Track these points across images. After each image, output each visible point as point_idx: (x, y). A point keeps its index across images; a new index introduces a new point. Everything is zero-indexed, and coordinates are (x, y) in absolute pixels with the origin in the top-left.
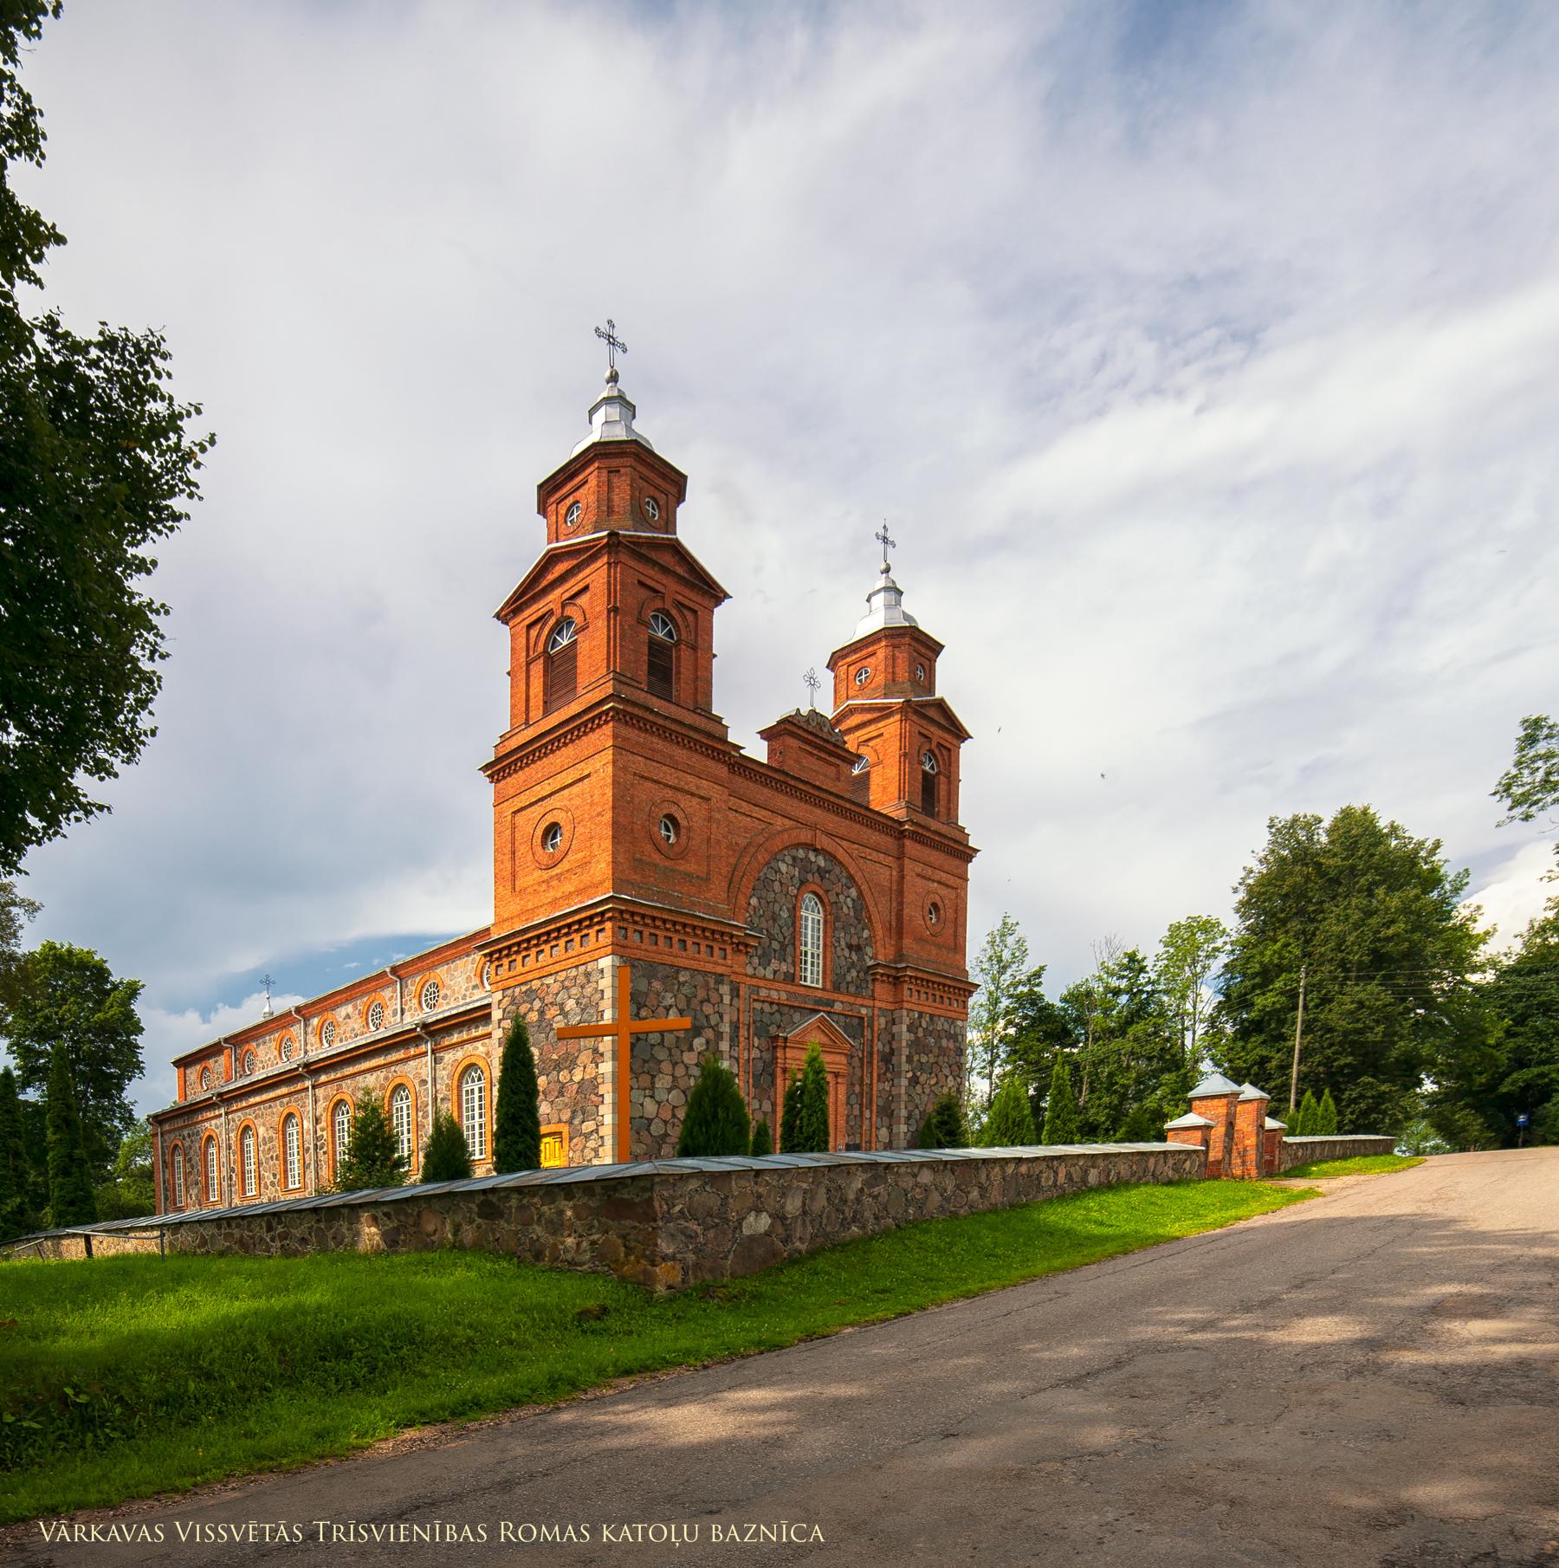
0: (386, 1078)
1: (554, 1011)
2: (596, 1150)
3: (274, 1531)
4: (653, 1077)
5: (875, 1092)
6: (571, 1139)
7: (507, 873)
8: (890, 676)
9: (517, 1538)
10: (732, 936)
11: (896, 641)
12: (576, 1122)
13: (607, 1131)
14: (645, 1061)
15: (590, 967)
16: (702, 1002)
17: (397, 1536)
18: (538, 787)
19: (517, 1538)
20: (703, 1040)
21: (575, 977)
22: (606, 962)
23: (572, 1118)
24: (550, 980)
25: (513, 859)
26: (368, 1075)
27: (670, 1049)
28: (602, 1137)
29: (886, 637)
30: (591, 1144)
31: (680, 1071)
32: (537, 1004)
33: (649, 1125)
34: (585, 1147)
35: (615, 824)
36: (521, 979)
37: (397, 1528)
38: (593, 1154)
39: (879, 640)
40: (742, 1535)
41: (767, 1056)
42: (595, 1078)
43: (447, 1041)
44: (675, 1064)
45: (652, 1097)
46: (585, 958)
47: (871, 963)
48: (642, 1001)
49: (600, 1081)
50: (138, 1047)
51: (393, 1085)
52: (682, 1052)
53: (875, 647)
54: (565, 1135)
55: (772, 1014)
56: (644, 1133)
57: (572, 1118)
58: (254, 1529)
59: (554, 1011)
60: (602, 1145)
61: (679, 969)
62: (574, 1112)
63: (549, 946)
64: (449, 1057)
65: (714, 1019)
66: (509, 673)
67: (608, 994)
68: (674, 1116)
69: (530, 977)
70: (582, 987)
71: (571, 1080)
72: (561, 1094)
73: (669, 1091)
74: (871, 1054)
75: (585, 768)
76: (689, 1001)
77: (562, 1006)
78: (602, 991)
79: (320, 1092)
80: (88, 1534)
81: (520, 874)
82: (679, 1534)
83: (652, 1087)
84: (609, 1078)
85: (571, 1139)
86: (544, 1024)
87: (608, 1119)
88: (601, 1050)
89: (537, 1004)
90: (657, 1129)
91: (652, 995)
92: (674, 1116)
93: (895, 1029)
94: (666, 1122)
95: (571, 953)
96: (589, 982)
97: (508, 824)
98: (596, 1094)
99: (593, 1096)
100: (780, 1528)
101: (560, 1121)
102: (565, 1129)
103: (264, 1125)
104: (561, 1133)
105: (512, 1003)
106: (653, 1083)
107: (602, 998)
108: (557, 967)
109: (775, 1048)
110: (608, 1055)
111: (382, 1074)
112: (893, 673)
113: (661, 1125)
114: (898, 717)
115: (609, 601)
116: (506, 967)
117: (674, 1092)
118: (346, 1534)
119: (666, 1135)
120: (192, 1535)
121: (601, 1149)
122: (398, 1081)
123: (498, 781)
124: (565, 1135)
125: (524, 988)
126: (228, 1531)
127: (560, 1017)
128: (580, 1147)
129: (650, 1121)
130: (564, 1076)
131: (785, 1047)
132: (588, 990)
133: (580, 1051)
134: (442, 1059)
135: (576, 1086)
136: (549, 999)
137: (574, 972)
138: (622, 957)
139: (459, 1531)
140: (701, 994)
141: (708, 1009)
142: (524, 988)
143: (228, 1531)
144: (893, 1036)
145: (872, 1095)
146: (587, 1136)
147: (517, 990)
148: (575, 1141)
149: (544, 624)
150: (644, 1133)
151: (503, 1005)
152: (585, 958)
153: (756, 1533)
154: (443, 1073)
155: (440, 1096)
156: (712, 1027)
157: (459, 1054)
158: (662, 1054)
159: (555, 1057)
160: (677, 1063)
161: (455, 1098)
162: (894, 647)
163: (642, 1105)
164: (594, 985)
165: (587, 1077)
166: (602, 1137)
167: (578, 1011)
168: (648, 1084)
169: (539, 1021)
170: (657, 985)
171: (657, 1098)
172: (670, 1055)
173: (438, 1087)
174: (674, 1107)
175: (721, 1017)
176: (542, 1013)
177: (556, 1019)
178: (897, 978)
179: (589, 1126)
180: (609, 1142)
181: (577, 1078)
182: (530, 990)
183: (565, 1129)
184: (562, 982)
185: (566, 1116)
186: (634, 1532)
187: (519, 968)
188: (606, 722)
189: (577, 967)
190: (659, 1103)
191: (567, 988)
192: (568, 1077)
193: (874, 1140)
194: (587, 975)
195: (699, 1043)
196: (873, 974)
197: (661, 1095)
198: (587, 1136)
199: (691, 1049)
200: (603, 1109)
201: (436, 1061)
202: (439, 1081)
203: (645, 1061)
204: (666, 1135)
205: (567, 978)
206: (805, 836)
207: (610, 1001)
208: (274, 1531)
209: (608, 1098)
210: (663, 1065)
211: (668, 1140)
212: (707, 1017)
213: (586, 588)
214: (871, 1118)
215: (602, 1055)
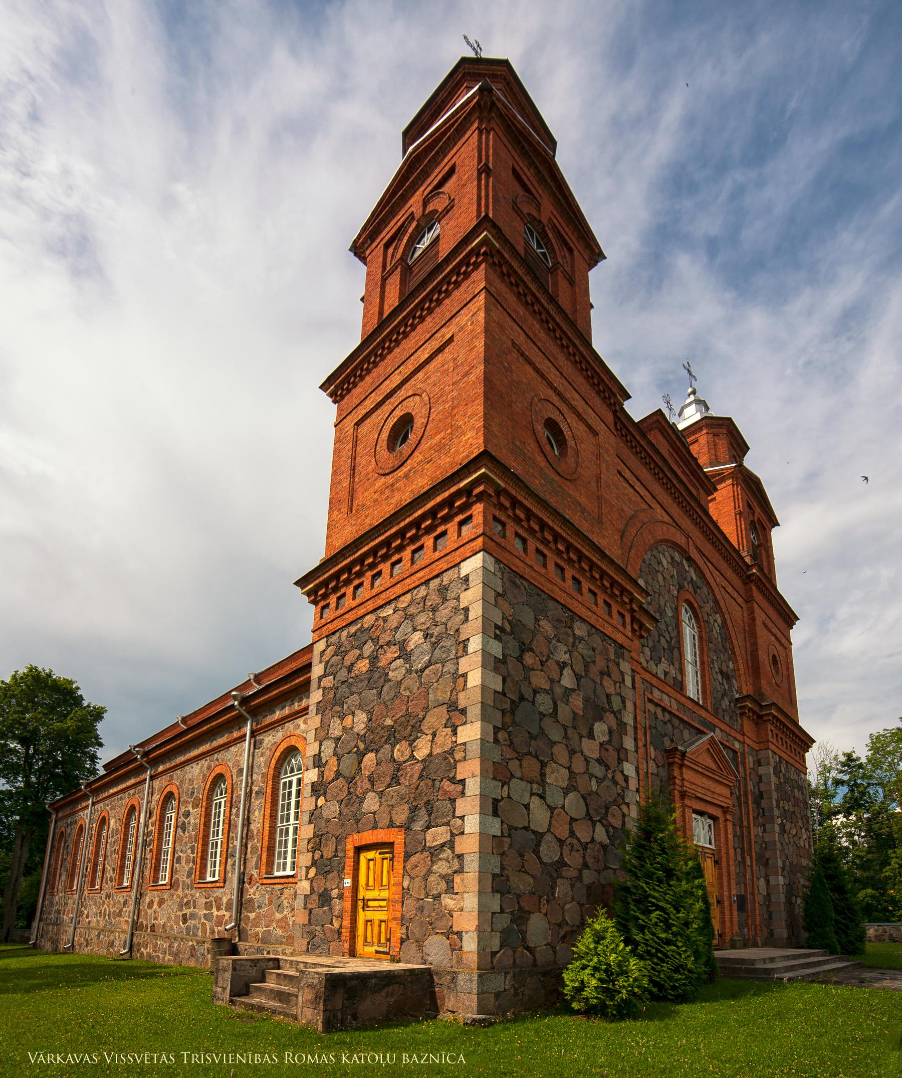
0: (209, 768)
1: (392, 652)
2: (449, 880)
3: (159, 1059)
4: (543, 765)
5: (752, 837)
6: (407, 856)
7: (344, 495)
8: (713, 457)
9: (294, 1061)
10: (632, 600)
11: (716, 431)
12: (417, 827)
13: (469, 845)
14: (532, 737)
15: (446, 578)
16: (602, 674)
17: (227, 1061)
18: (387, 382)
19: (294, 1061)
20: (605, 727)
21: (424, 599)
22: (473, 565)
23: (411, 820)
24: (388, 611)
25: (353, 476)
26: (194, 765)
27: (565, 728)
28: (460, 857)
29: (707, 426)
30: (441, 867)
31: (579, 766)
32: (369, 649)
33: (538, 844)
34: (429, 872)
35: (488, 379)
36: (350, 617)
37: (227, 1057)
38: (443, 886)
39: (700, 429)
40: (420, 1058)
41: (663, 773)
42: (451, 752)
43: (269, 719)
44: (572, 752)
45: (542, 797)
46: (442, 565)
47: (737, 696)
48: (527, 642)
49: (458, 756)
50: (97, 758)
51: (213, 775)
52: (581, 737)
53: (696, 436)
54: (399, 849)
55: (665, 723)
56: (530, 856)
57: (411, 820)
58: (148, 1056)
59: (392, 652)
60: (460, 871)
61: (574, 616)
62: (414, 810)
63: (388, 564)
64: (268, 739)
65: (616, 702)
66: (362, 299)
67: (476, 611)
68: (572, 834)
69: (361, 611)
70: (434, 610)
71: (412, 757)
72: (395, 780)
73: (566, 792)
74: (746, 794)
75: (447, 333)
76: (586, 666)
77: (403, 645)
78: (466, 610)
79: (157, 783)
80: (55, 1059)
81: (359, 489)
82: (385, 1058)
83: (542, 782)
84: (475, 750)
85: (407, 856)
86: (376, 675)
87: (472, 824)
88: (462, 704)
89: (369, 649)
90: (549, 852)
91: (540, 638)
92: (572, 834)
93: (762, 770)
94: (561, 842)
95: (419, 564)
96: (445, 600)
97: (350, 438)
98: (453, 780)
99: (446, 784)
100: (441, 1055)
101: (391, 825)
102: (398, 838)
103: (115, 817)
104: (391, 845)
105: (336, 654)
106: (543, 775)
107: (466, 620)
108: (398, 590)
109: (670, 765)
110: (475, 711)
111: (204, 763)
112: (716, 455)
113: (555, 845)
114: (729, 482)
115: (480, 161)
116: (333, 605)
117: (572, 796)
118: (199, 1059)
119: (561, 863)
120: (113, 1060)
121: (457, 879)
122: (218, 770)
123: (343, 397)
124: (399, 849)
125: (353, 629)
126: (133, 1057)
127: (400, 662)
128: (421, 870)
129: (539, 836)
130: (400, 751)
131: (681, 766)
132: (443, 614)
133: (426, 709)
134: (262, 741)
135: (419, 767)
136: (386, 637)
137: (423, 591)
138: (498, 561)
139: (410, 1057)
140: (601, 664)
141: (608, 683)
142: (353, 629)
143: (133, 1057)
144: (760, 777)
145: (750, 839)
146: (434, 853)
147: (345, 633)
148: (414, 859)
149: (401, 240)
150: (530, 856)
151: (326, 658)
152: (442, 565)
153: (428, 1059)
154: (261, 760)
155: (255, 789)
156: (613, 712)
157: (279, 735)
158: (555, 734)
159: (389, 722)
160: (575, 752)
161: (269, 791)
162: (715, 435)
163: (527, 807)
164: (452, 603)
165: (437, 751)
166: (460, 857)
167: (427, 647)
168: (535, 774)
169: (370, 671)
170: (546, 626)
171: (549, 800)
172: (566, 736)
173: (255, 777)
174: (573, 820)
175: (624, 702)
176: (374, 659)
177: (393, 665)
178: (760, 717)
179: (437, 835)
180: (472, 865)
181: (420, 754)
182: (361, 630)
183: (398, 838)
184: (405, 609)
185: (401, 817)
186: (360, 1059)
187: (348, 602)
188: (476, 266)
189: (427, 583)
190: (552, 809)
191: (412, 616)
192: (407, 753)
193: (756, 892)
194: (443, 591)
195: (600, 729)
196: (741, 708)
197: (553, 796)
198: (434, 853)
199: (591, 736)
200: (462, 806)
201: (256, 745)
202: (256, 770)
203: (532, 737)
204: (561, 863)
205: (412, 601)
206: (680, 539)
207: (478, 659)
208: (159, 1059)
209: (473, 787)
210: (557, 749)
211: (565, 872)
212: (608, 696)
213: (452, 171)
214: (751, 866)
215: (463, 712)
